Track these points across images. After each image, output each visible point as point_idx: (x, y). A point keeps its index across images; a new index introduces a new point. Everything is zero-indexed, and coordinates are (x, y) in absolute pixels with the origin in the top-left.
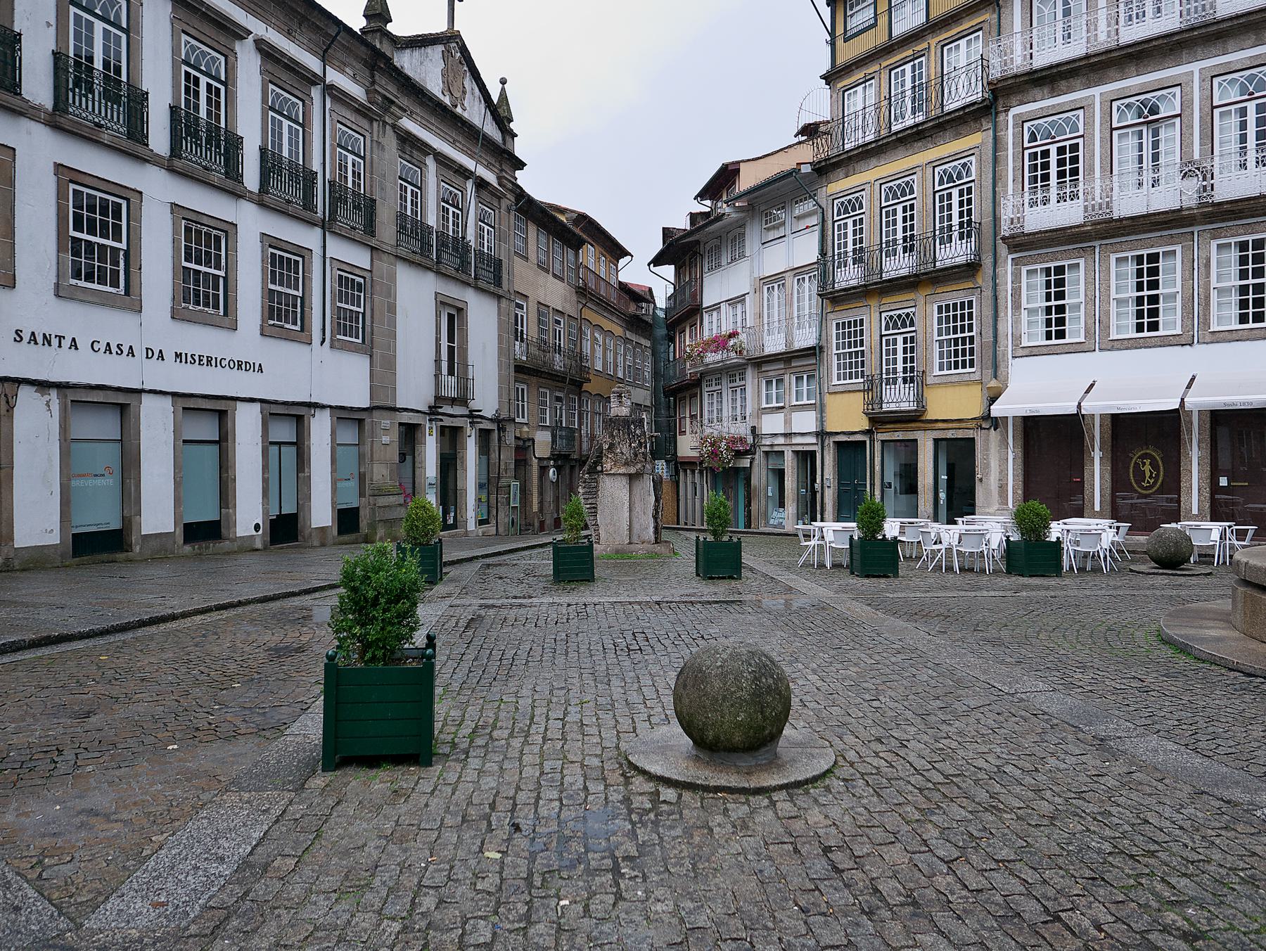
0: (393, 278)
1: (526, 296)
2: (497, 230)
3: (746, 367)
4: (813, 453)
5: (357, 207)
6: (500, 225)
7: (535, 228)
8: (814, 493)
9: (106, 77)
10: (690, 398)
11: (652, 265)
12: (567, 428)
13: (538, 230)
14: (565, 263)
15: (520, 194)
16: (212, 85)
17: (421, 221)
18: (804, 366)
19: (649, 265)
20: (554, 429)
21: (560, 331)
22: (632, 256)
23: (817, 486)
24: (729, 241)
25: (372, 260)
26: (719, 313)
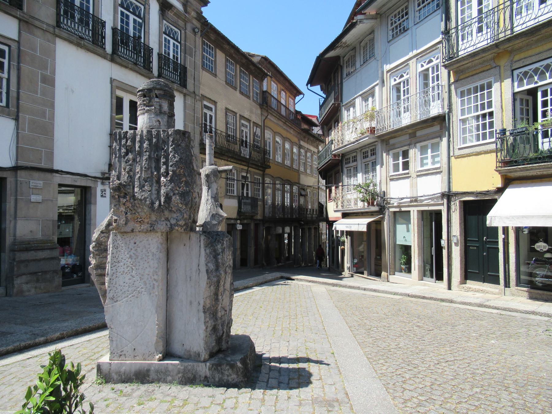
0: (51, 54)
1: (214, 101)
2: (183, 45)
3: (376, 143)
4: (438, 214)
6: (185, 41)
7: (223, 55)
8: (439, 249)
10: (335, 174)
11: (309, 85)
12: (251, 198)
13: (227, 60)
14: (251, 88)
15: (205, 23)
18: (504, 20)
19: (307, 85)
21: (246, 133)
22: (304, 95)
23: (444, 243)
24: (362, 48)
26: (354, 107)
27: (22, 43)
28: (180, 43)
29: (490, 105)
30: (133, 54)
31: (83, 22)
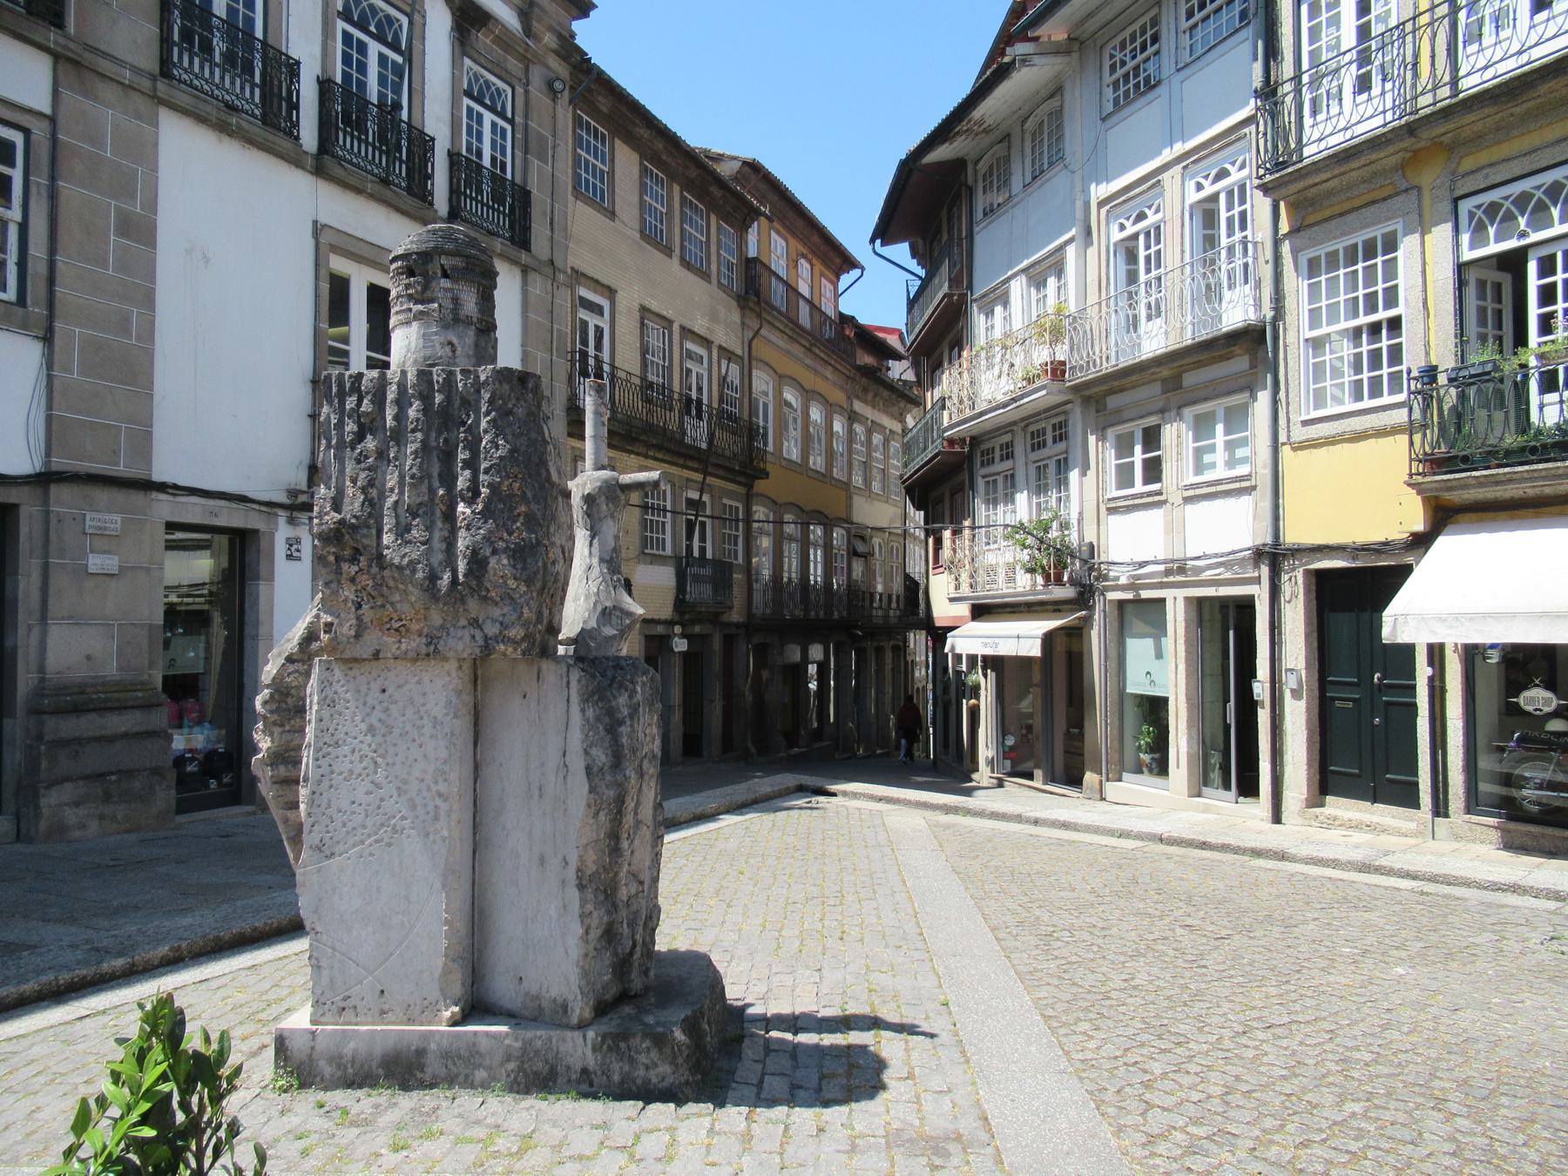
0: (146, 153)
1: (609, 288)
2: (520, 129)
5: (498, 197)
6: (526, 117)
7: (634, 157)
9: (493, 175)
12: (714, 561)
13: (644, 171)
14: (713, 249)
15: (582, 66)
16: (387, 58)
17: (409, 124)
20: (684, 566)
21: (699, 377)
22: (863, 269)
25: (56, 93)
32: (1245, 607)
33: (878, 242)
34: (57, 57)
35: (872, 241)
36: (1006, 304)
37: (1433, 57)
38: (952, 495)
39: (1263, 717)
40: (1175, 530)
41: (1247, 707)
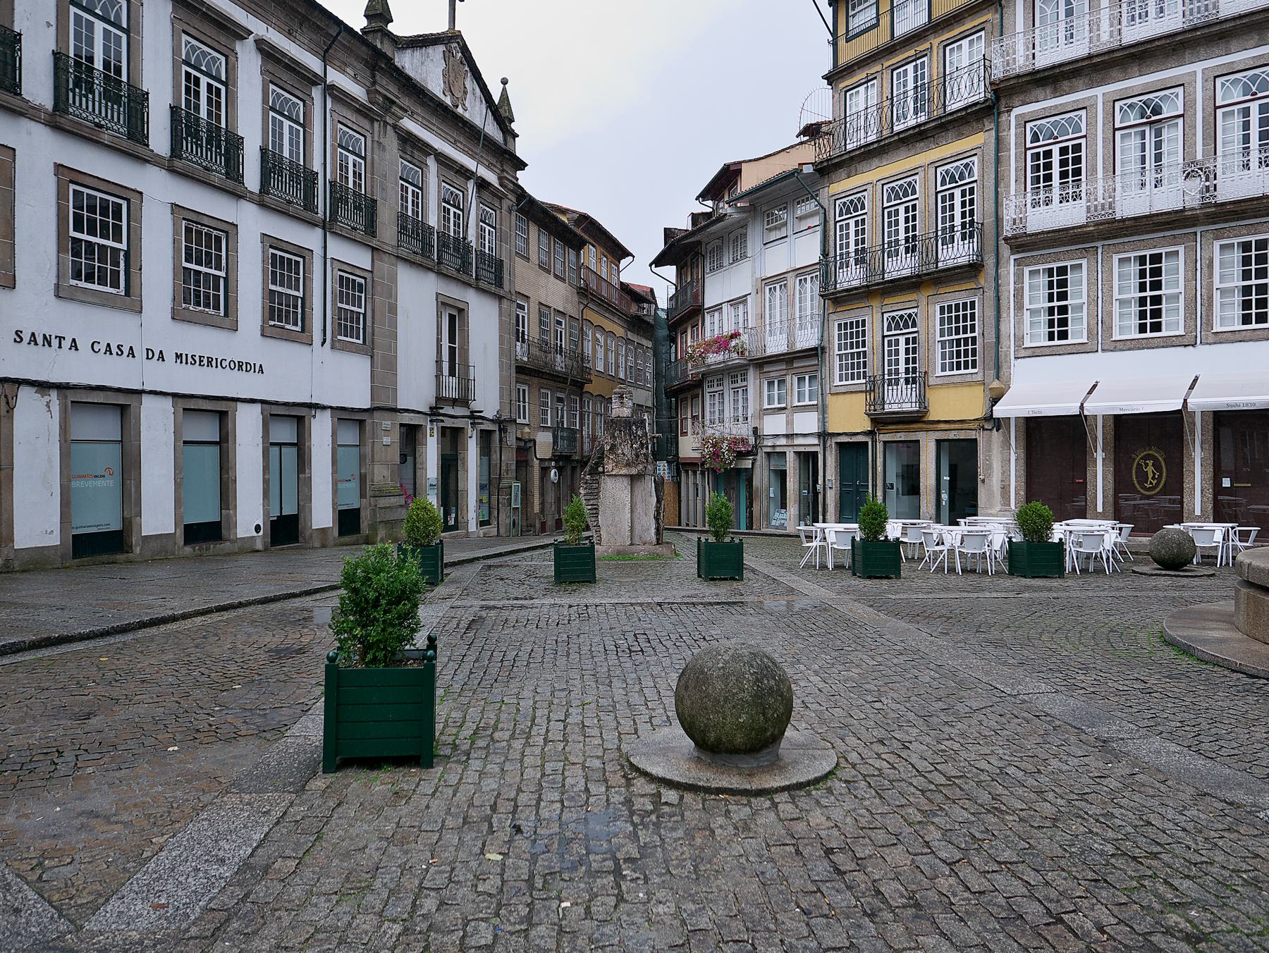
0: (393, 279)
1: (527, 297)
2: (498, 231)
6: (501, 225)
7: (536, 228)
12: (568, 428)
13: (539, 230)
14: (567, 264)
15: (521, 194)
22: (634, 257)
27: (375, 273)
28: (364, 158)
29: (973, 330)
30: (194, 146)
31: (111, 96)
32: (815, 454)
33: (653, 266)
34: (374, 249)
35: (650, 265)
36: (721, 313)
37: (806, 366)
38: (692, 399)
39: (820, 497)
40: (790, 423)
41: (816, 494)
